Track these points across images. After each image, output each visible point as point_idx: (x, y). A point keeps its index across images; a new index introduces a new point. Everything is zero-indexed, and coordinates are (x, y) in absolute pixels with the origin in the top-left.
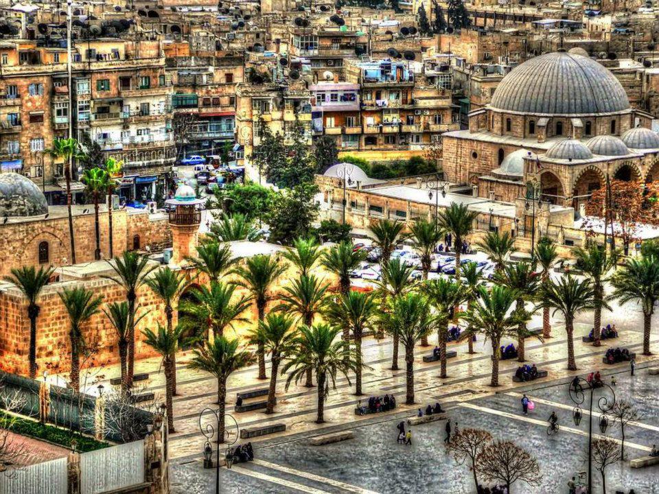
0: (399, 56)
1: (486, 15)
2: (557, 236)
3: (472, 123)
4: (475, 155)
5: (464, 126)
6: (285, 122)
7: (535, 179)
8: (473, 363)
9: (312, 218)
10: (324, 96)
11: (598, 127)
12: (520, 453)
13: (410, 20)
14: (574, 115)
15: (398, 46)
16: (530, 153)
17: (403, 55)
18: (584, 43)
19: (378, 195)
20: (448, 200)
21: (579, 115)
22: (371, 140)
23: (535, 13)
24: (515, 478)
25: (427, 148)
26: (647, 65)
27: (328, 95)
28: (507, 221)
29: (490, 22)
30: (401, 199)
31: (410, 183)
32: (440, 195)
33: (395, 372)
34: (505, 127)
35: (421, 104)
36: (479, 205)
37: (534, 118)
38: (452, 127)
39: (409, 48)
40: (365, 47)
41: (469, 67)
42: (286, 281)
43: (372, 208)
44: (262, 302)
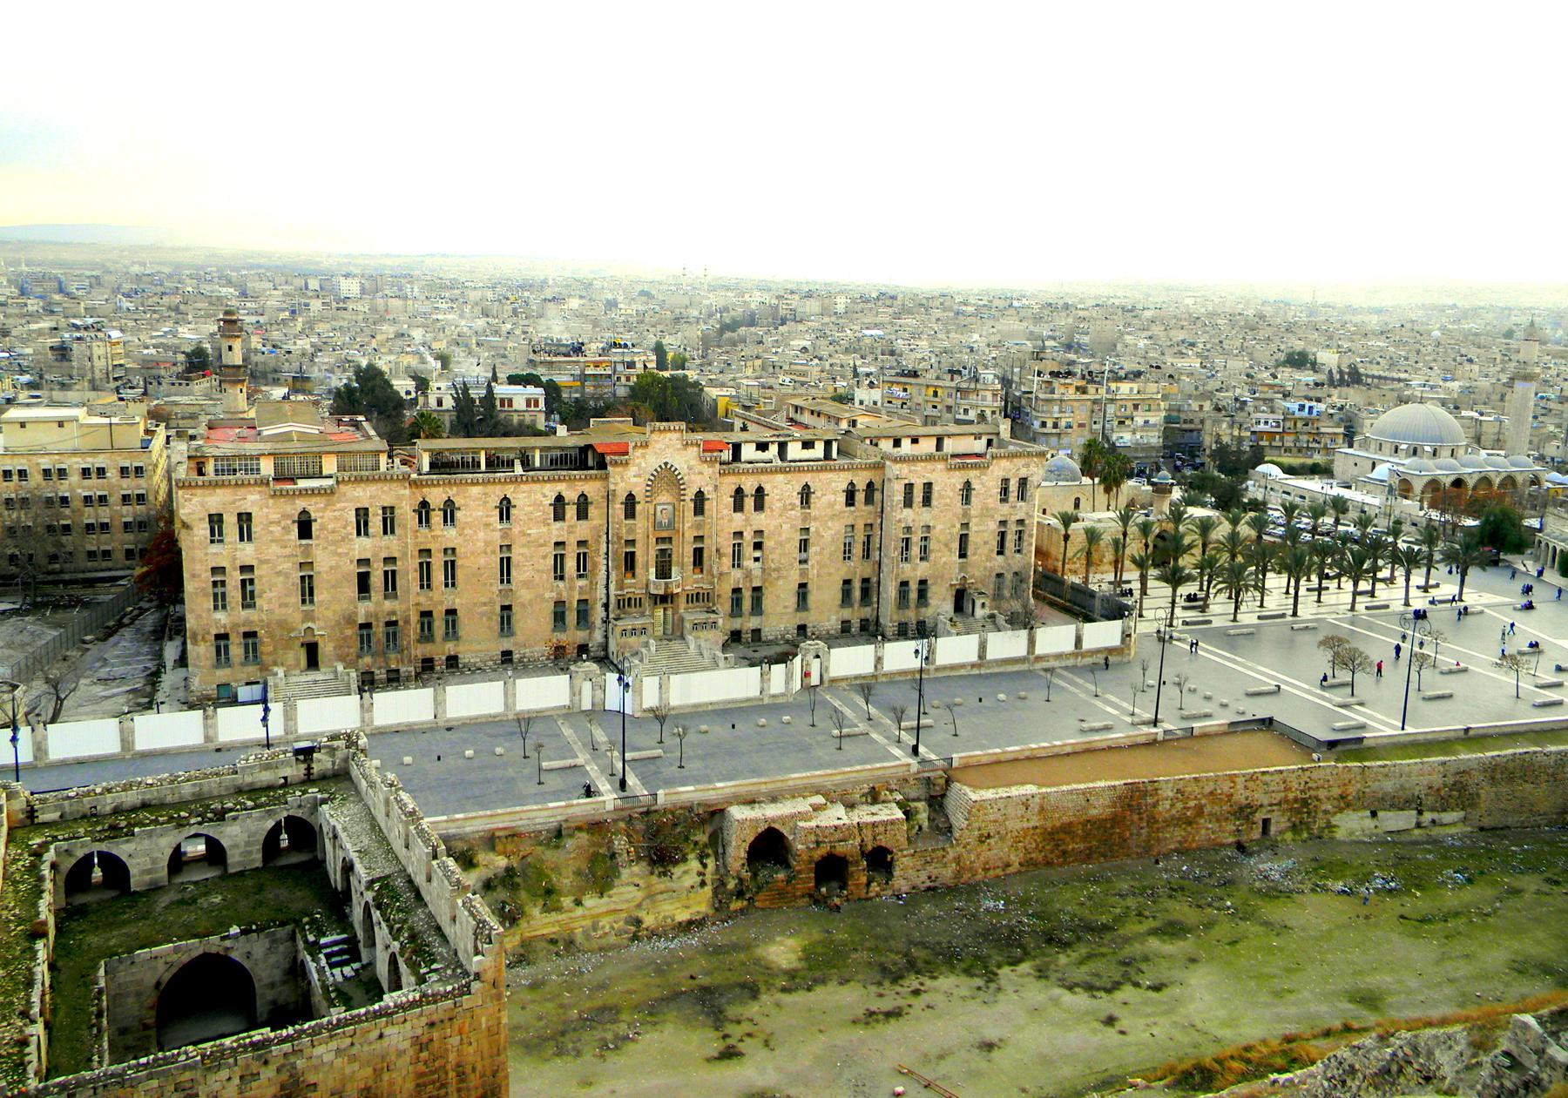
1: (1373, 377)
5: (1351, 446)
15: (1312, 394)
22: (1288, 450)
26: (1482, 414)
35: (1323, 430)
42: (1222, 531)
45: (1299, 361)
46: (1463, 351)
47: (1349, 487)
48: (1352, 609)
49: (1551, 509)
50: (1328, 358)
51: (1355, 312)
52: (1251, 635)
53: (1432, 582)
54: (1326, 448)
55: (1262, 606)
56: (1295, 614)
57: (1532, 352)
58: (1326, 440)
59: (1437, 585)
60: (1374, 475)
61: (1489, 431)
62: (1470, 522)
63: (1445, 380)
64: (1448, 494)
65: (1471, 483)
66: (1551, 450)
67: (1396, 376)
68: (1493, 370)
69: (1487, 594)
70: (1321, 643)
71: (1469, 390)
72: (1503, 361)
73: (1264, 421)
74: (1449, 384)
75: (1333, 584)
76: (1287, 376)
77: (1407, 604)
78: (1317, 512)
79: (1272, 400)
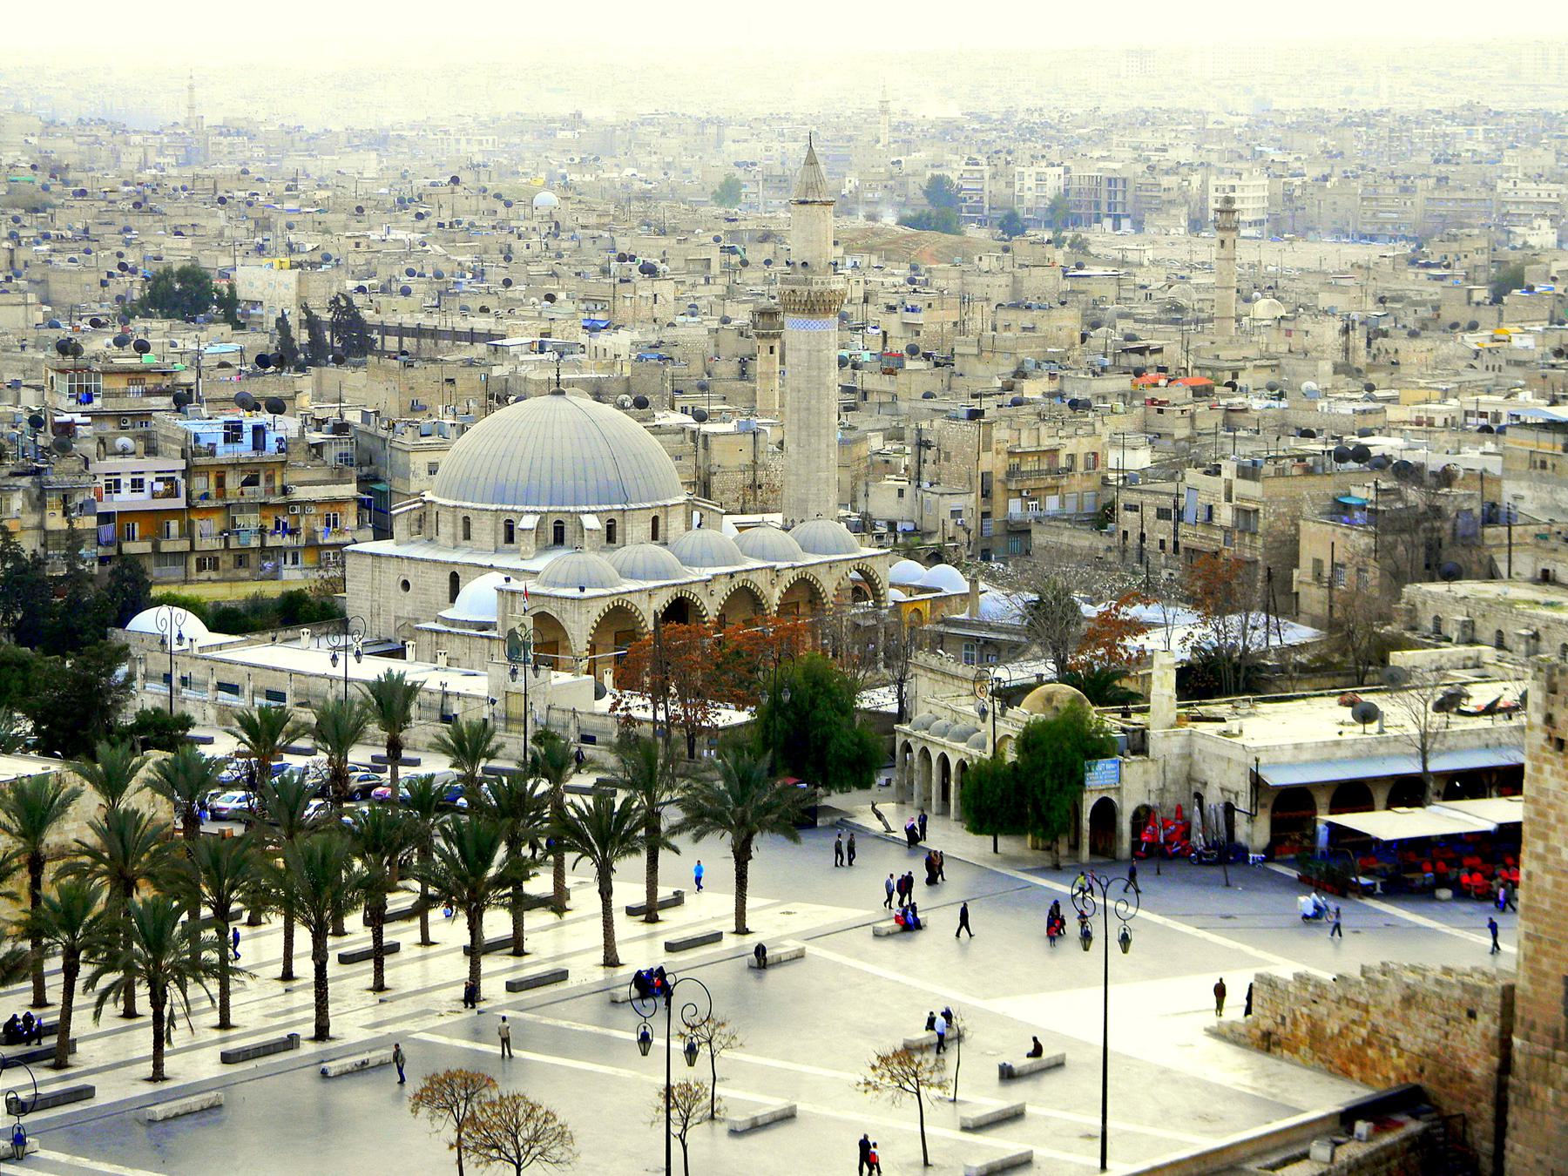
0: (258, 408)
1: (401, 331)
2: (566, 727)
3: (399, 528)
4: (406, 585)
5: (383, 532)
6: (47, 533)
7: (523, 625)
8: (431, 962)
9: (118, 705)
10: (117, 482)
11: (628, 527)
12: (540, 1112)
13: (262, 342)
14: (586, 508)
15: (255, 388)
16: (508, 580)
17: (262, 404)
18: (584, 380)
19: (230, 662)
20: (373, 669)
21: (593, 508)
22: (208, 562)
23: (493, 327)
24: (529, 1158)
25: (315, 575)
26: (701, 417)
27: (126, 480)
28: (475, 704)
29: (409, 343)
30: (275, 669)
31: (286, 640)
32: (352, 659)
33: (288, 985)
34: (460, 533)
35: (300, 494)
36: (411, 670)
37: (513, 517)
38: (359, 535)
39: (273, 392)
40: (190, 391)
41: (385, 425)
42: (79, 824)
43: (221, 686)
44: (36, 865)
45: (188, 296)
46: (624, 245)
47: (399, 653)
48: (472, 995)
49: (921, 657)
50: (269, 285)
51: (314, 143)
52: (210, 1112)
53: (664, 892)
54: (313, 545)
55: (224, 1024)
56: (322, 1033)
57: (814, 236)
58: (312, 522)
59: (678, 900)
60: (461, 610)
61: (730, 457)
62: (730, 716)
63: (592, 328)
64: (658, 646)
65: (711, 607)
66: (885, 501)
67: (462, 325)
68: (707, 294)
69: (807, 904)
70: (420, 1099)
71: (658, 354)
72: (728, 269)
73: (131, 481)
74: (603, 340)
75: (403, 934)
76: (169, 341)
77: (611, 961)
78: (336, 730)
79: (144, 416)
